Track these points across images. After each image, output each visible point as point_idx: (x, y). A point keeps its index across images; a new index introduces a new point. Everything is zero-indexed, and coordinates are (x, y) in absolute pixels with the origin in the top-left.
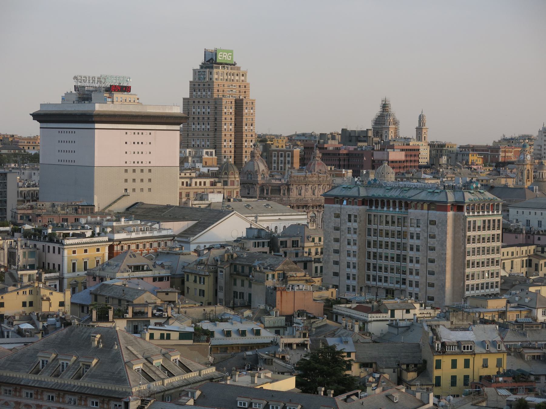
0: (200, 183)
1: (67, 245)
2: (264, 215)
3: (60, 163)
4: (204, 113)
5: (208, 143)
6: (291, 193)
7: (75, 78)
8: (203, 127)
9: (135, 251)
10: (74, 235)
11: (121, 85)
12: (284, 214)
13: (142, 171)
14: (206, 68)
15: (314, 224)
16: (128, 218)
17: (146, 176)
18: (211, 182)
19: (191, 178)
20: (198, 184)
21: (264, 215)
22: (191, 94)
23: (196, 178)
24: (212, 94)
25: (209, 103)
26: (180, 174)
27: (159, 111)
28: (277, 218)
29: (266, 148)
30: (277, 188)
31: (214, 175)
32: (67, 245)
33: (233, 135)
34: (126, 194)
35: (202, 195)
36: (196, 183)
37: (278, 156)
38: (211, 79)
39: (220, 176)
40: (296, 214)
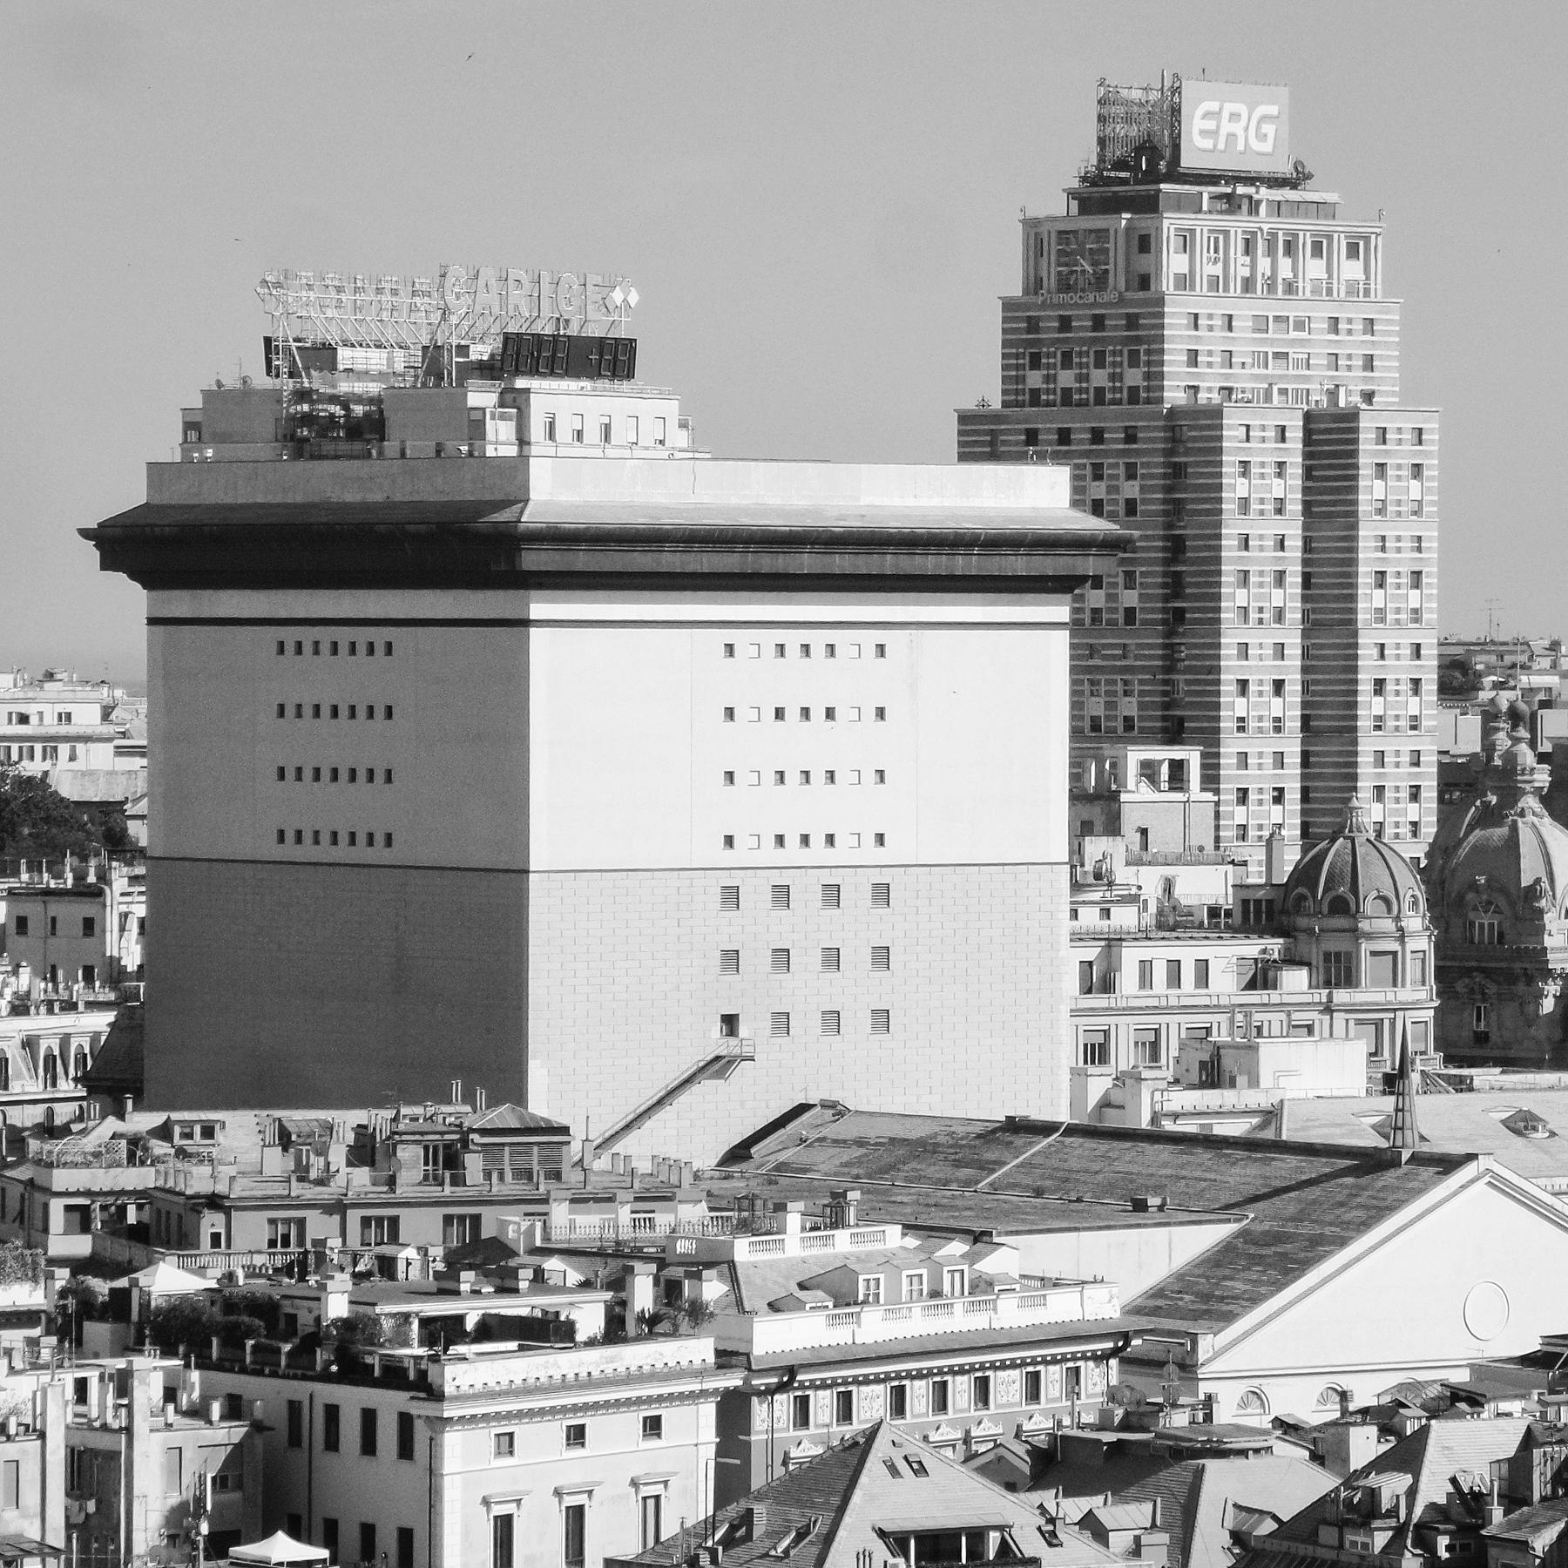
0: (1175, 967)
3: (290, 851)
10: (490, 1329)
11: (573, 331)
13: (832, 894)
14: (1113, 205)
19: (1113, 942)
20: (1160, 973)
22: (1013, 380)
23: (1144, 936)
24: (1155, 377)
25: (1131, 437)
26: (1075, 914)
27: (936, 502)
31: (1262, 912)
36: (1145, 967)
38: (1144, 282)
39: (1302, 922)
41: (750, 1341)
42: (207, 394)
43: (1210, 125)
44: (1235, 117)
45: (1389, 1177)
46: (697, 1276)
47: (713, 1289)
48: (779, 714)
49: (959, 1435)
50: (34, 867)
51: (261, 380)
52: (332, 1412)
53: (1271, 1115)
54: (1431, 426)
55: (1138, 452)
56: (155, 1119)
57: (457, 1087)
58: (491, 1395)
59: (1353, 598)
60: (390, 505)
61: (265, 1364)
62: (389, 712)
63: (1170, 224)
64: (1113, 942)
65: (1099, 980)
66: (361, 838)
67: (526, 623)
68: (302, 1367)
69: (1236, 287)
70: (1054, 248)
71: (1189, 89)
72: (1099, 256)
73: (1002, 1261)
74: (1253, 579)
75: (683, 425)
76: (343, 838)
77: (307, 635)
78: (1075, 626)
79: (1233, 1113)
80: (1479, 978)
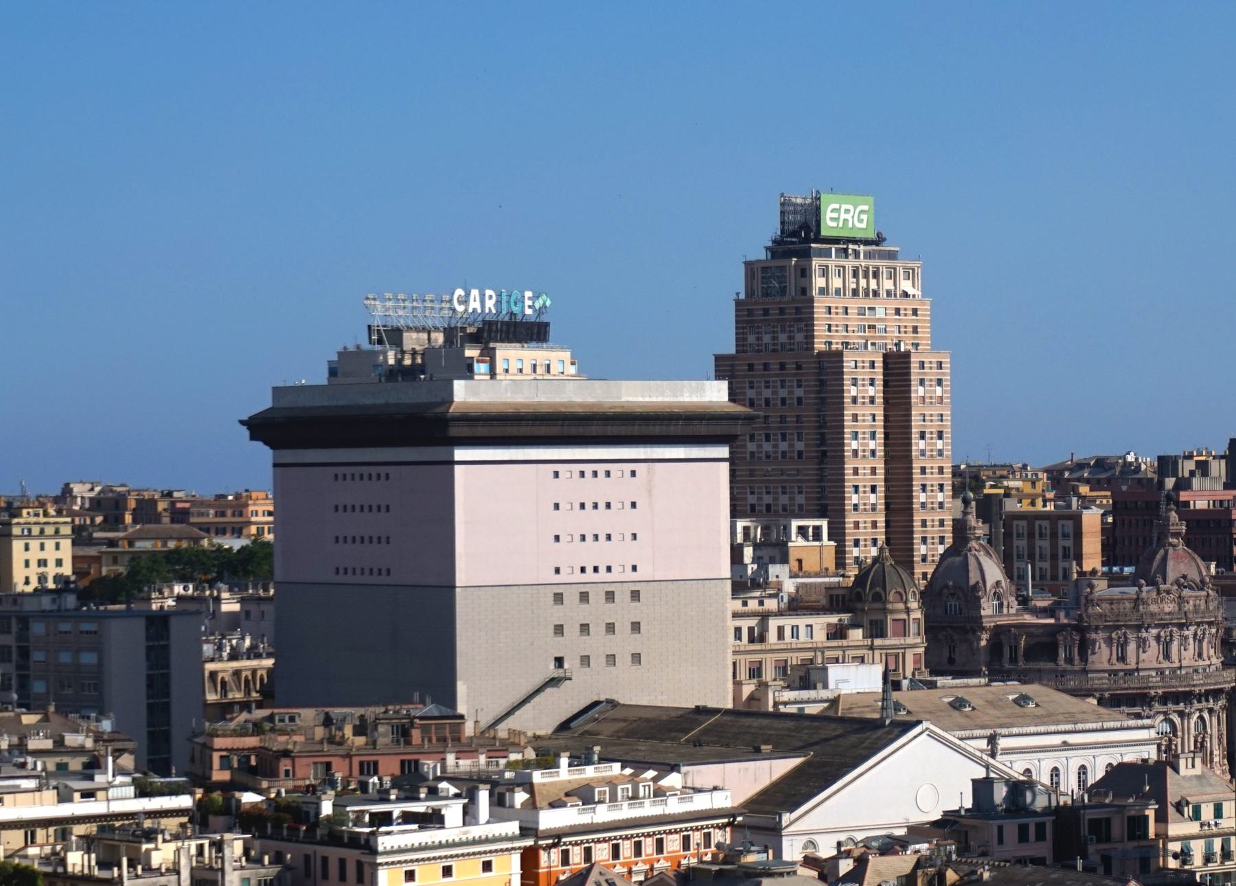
1: (386, 853)
2: (1015, 730)
3: (341, 578)
4: (783, 401)
5: (800, 499)
6: (1091, 658)
8: (783, 446)
9: (607, 866)
10: (408, 818)
12: (1080, 726)
13: (610, 596)
14: (788, 254)
15: (1198, 761)
16: (580, 759)
17: (623, 612)
18: (829, 625)
19: (764, 617)
21: (1015, 730)
23: (780, 613)
24: (810, 337)
25: (799, 367)
27: (660, 399)
28: (1057, 740)
29: (988, 509)
30: (1045, 639)
31: (836, 601)
32: (386, 853)
33: (881, 471)
35: (808, 671)
36: (781, 630)
39: (859, 606)
40: (1118, 724)
41: (537, 823)
42: (340, 354)
43: (835, 215)
44: (847, 211)
45: (879, 733)
46: (513, 791)
47: (520, 797)
48: (582, 506)
49: (626, 870)
50: (255, 587)
51: (366, 346)
52: (325, 860)
53: (834, 702)
54: (946, 361)
55: (802, 375)
56: (265, 712)
57: (416, 696)
58: (401, 851)
59: (910, 444)
60: (387, 405)
61: (293, 837)
62: (337, 508)
63: (816, 263)
64: (764, 617)
65: (758, 637)
67: (453, 463)
68: (310, 838)
69: (849, 293)
71: (824, 198)
72: (782, 279)
73: (673, 780)
74: (860, 436)
75: (573, 363)
78: (732, 460)
79: (815, 701)
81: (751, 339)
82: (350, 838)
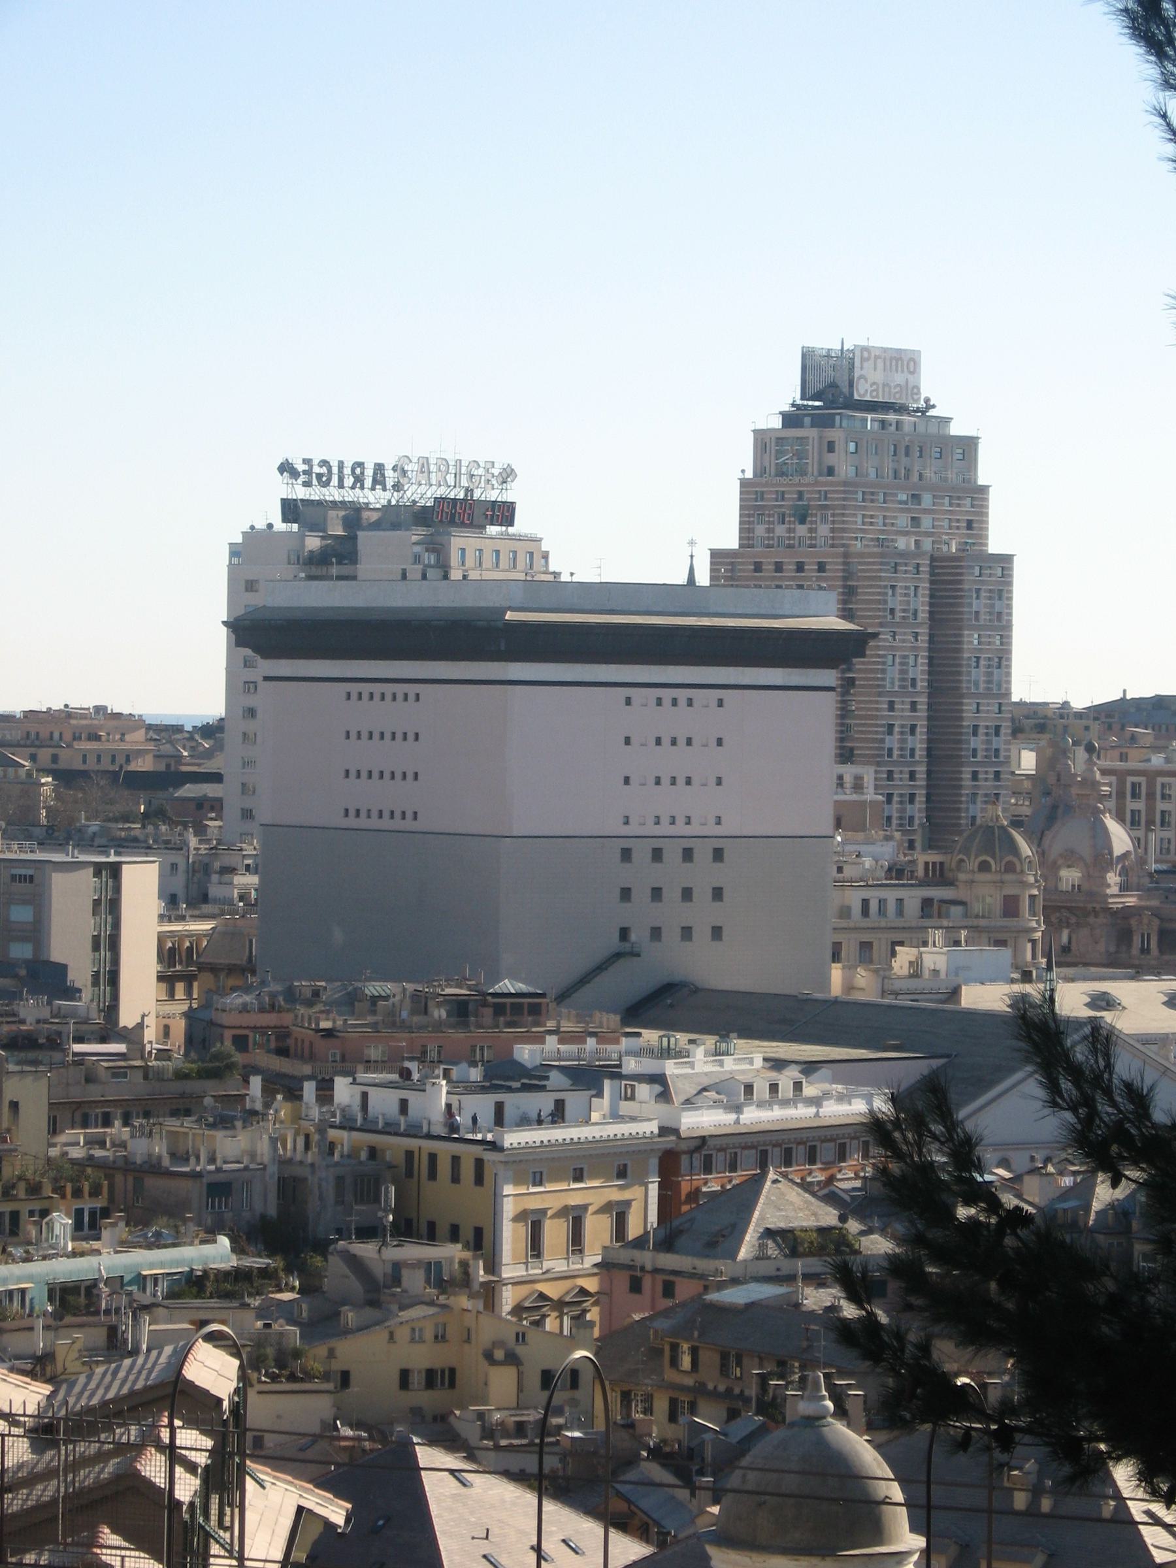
3: (351, 822)
7: (286, 468)
13: (688, 855)
17: (703, 874)
20: (891, 907)
34: (626, 946)
37: (1151, 796)
51: (280, 526)
66: (398, 815)
70: (774, 448)
72: (800, 455)
76: (386, 814)
77: (366, 688)
80: (1066, 914)
81: (760, 530)
82: (48, 1038)
